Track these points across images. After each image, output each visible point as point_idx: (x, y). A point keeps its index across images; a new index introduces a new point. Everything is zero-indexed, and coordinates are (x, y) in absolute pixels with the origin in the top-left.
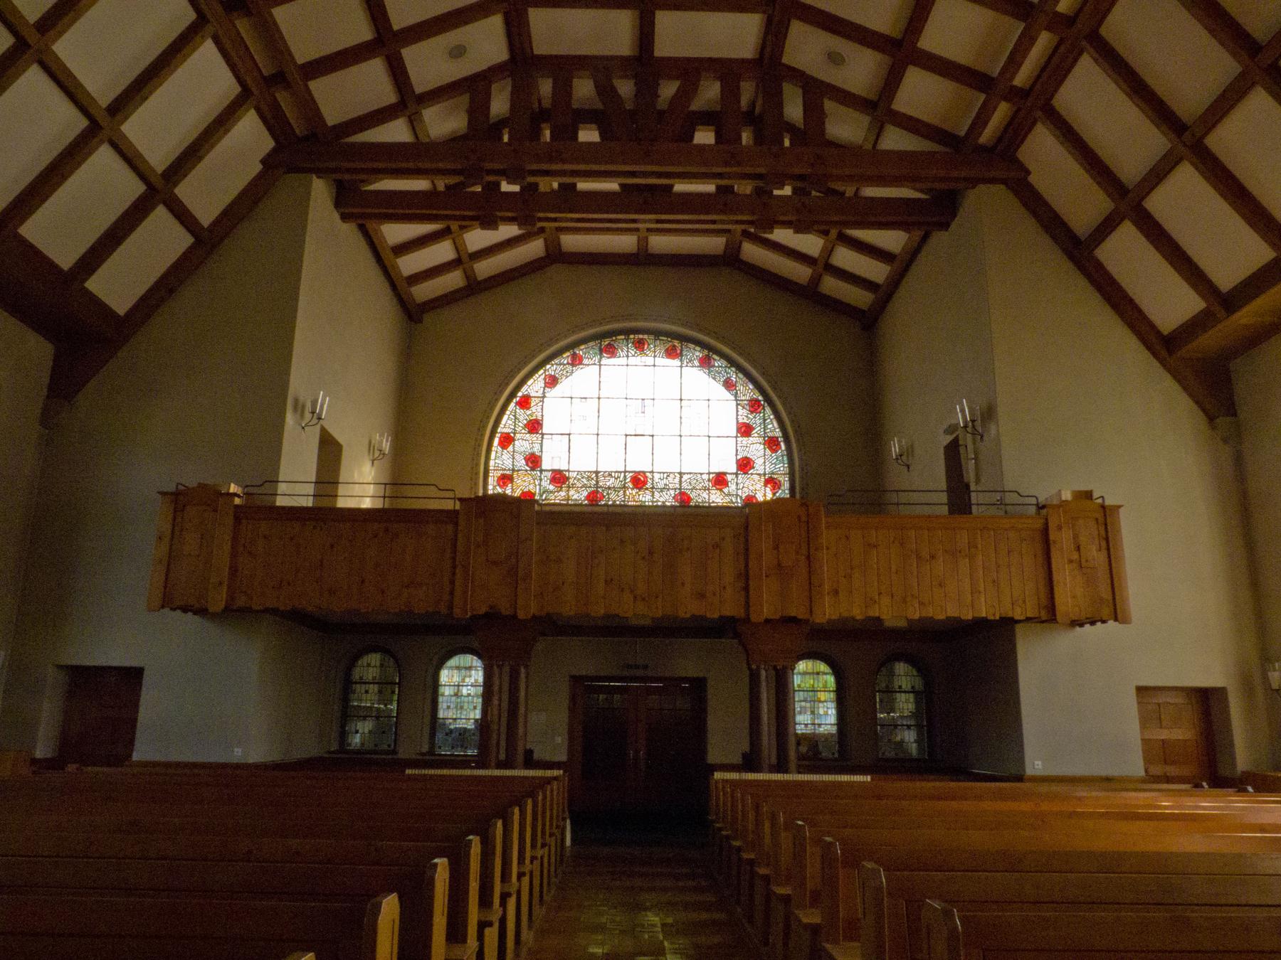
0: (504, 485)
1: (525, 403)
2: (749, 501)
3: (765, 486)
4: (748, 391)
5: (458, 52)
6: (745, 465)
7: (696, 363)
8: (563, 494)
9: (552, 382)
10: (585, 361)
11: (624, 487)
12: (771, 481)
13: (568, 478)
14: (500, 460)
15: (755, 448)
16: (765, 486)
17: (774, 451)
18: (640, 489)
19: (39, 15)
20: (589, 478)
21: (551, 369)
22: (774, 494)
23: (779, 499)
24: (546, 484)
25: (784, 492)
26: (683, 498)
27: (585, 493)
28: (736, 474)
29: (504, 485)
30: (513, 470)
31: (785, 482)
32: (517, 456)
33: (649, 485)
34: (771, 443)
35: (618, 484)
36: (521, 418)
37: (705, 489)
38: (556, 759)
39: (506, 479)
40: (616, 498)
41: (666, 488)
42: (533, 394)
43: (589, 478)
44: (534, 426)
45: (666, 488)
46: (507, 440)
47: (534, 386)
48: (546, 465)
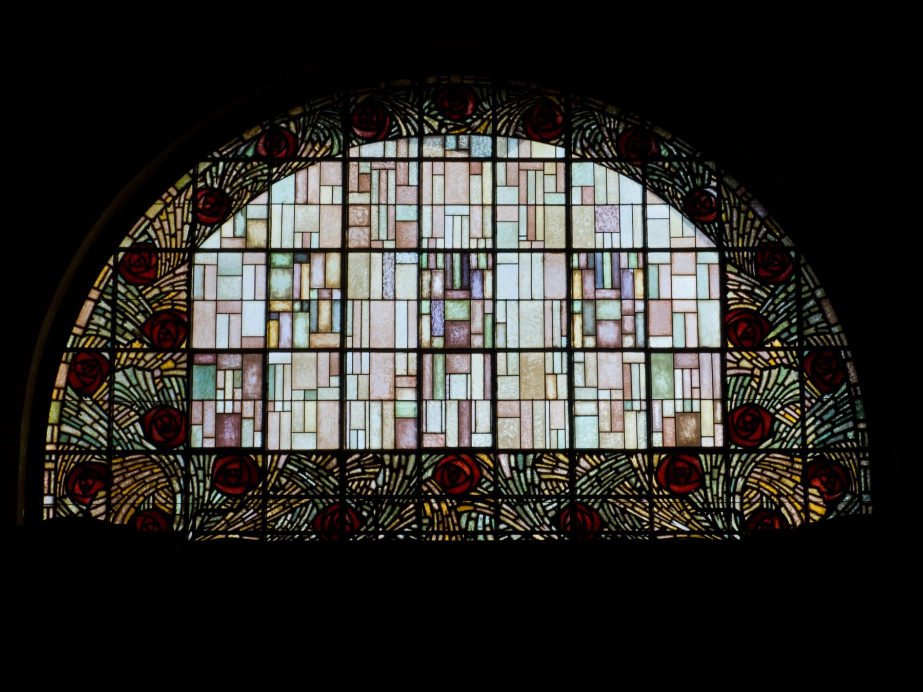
0: (84, 497)
1: (142, 265)
2: (768, 516)
3: (806, 483)
4: (752, 226)
5: (539, 439)
6: (746, 424)
7: (608, 150)
8: (249, 515)
9: (215, 209)
10: (306, 151)
11: (420, 497)
12: (820, 469)
13: (264, 472)
14: (73, 424)
15: (778, 380)
16: (806, 483)
17: (828, 387)
18: (462, 498)
19: (499, 383)
20: (320, 472)
21: (212, 173)
22: (830, 506)
23: (843, 518)
24: (200, 487)
25: (857, 500)
26: (575, 514)
27: (310, 513)
28: (724, 452)
29: (84, 497)
30: (111, 452)
31: (859, 465)
32: (120, 413)
33: (486, 487)
34: (817, 367)
35: (399, 487)
36: (131, 308)
37: (640, 495)
38: (500, 441)
39: (90, 476)
40: (399, 524)
41: (532, 495)
42: (162, 242)
43: (320, 472)
44: (170, 329)
45: (532, 495)
46: (93, 371)
47: (165, 220)
48: (202, 435)
